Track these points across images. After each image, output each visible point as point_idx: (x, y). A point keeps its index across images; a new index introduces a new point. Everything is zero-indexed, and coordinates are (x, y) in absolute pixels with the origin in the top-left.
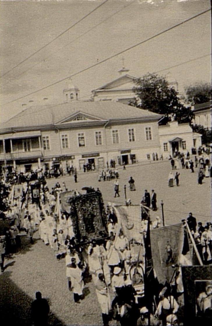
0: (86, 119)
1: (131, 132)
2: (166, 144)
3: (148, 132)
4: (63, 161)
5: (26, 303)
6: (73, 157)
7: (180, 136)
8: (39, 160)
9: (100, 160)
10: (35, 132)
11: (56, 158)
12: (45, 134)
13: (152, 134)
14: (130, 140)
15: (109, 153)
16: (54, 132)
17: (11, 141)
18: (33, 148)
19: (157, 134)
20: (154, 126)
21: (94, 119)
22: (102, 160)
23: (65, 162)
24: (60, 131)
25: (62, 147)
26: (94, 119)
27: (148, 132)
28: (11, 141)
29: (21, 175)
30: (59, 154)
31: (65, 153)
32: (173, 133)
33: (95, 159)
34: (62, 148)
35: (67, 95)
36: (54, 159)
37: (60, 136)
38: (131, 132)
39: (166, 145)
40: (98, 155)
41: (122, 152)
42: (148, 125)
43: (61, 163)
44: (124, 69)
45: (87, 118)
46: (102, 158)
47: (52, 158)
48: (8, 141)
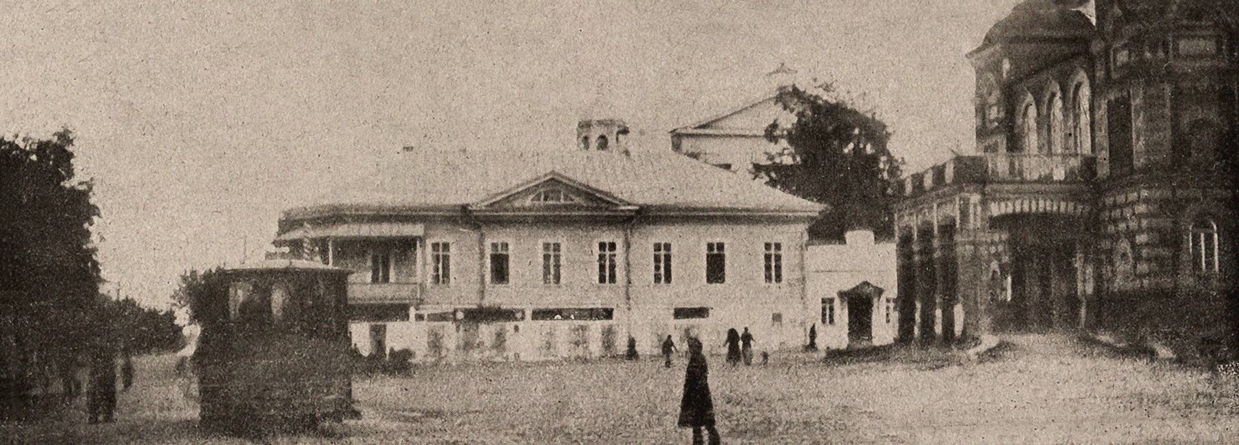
2: (831, 300)
6: (519, 315)
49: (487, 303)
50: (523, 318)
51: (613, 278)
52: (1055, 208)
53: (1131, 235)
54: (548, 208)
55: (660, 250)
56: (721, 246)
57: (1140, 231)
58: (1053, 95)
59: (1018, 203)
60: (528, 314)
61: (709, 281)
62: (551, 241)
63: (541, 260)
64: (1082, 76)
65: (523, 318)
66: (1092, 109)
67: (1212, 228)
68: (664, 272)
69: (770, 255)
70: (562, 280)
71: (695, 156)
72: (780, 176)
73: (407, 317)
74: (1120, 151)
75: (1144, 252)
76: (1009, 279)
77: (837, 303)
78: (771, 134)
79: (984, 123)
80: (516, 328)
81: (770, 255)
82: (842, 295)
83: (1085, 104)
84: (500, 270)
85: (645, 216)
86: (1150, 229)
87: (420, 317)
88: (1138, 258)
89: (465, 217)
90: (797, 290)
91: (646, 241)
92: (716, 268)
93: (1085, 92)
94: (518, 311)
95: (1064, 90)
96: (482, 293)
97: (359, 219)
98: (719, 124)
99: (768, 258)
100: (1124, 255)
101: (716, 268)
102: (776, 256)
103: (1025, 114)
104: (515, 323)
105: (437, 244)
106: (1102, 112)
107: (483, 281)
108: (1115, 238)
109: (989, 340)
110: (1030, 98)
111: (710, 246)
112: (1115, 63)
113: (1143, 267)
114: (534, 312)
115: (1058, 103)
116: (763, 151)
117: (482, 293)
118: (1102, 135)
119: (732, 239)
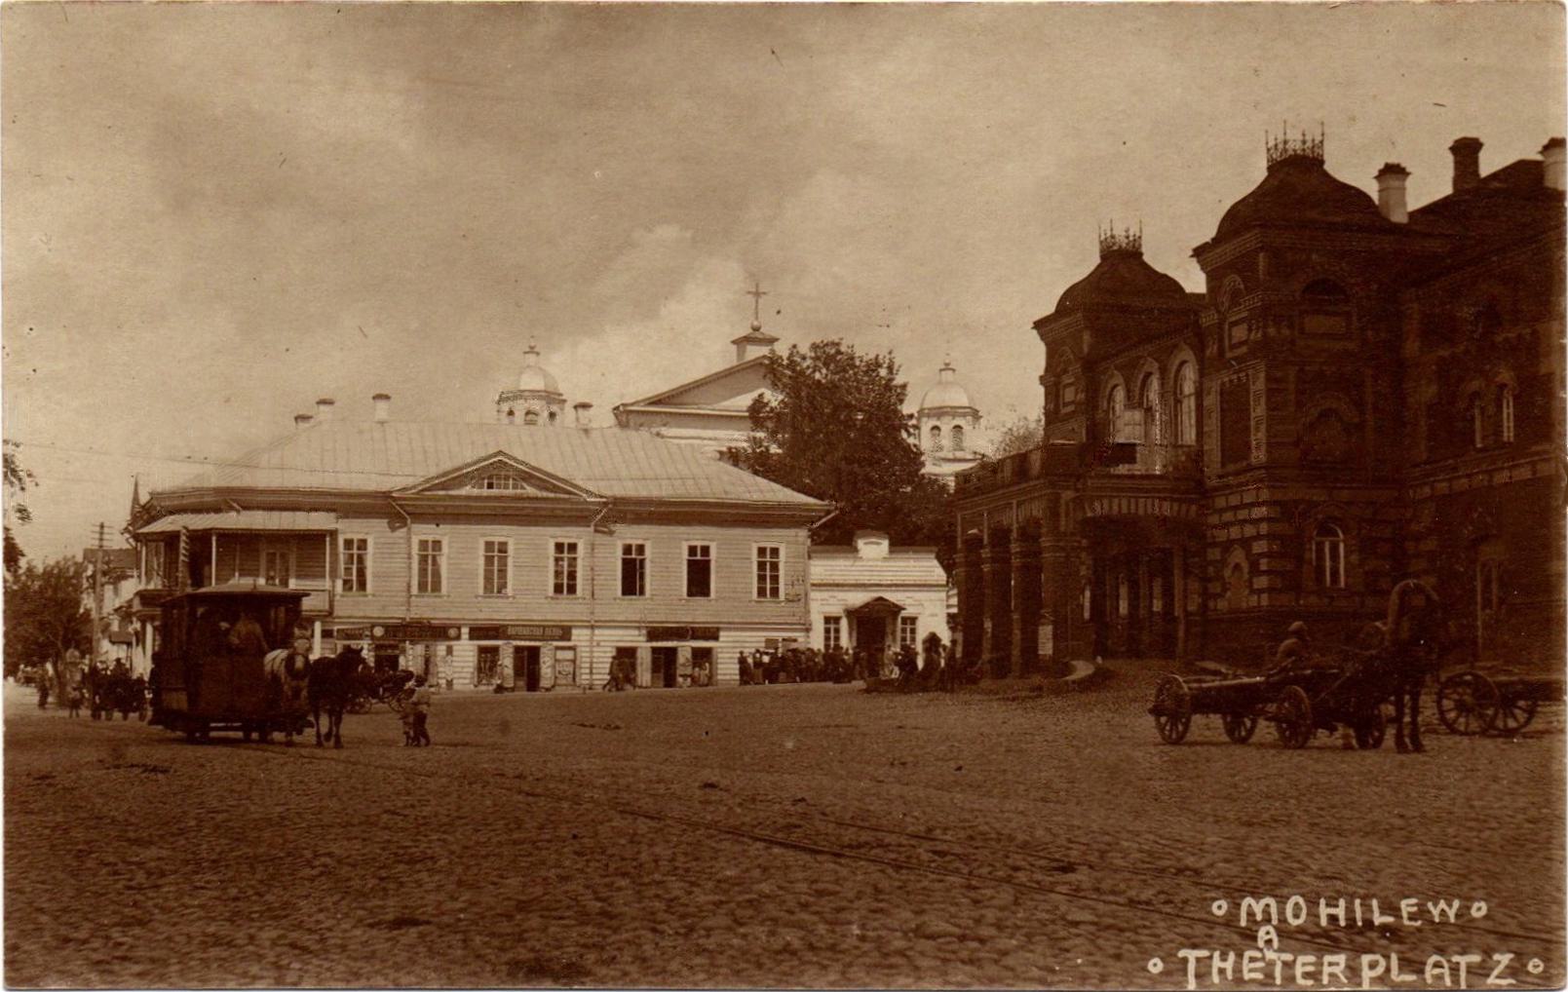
0: (523, 488)
1: (497, 555)
2: (837, 620)
3: (768, 566)
4: (412, 642)
5: (1271, 964)
6: (452, 632)
7: (892, 597)
8: (318, 627)
9: (560, 655)
10: (275, 514)
11: (387, 627)
12: (350, 529)
13: (781, 573)
14: (558, 589)
15: (597, 632)
16: (384, 522)
17: (214, 538)
18: (298, 577)
19: (801, 578)
20: (790, 543)
21: (601, 497)
22: (569, 655)
23: (420, 649)
24: (412, 522)
25: (415, 583)
26: (601, 497)
27: (768, 566)
28: (214, 538)
29: (758, 655)
30: (397, 613)
31: (426, 609)
32: (865, 579)
33: (542, 650)
34: (415, 590)
35: (936, 428)
36: (378, 632)
37: (409, 540)
38: (497, 555)
39: (832, 627)
40: (565, 633)
41: (654, 634)
42: (771, 537)
43: (404, 651)
44: (757, 335)
45: (525, 485)
46: (573, 648)
47: (373, 626)
48: (200, 538)
50: (458, 637)
52: (1115, 508)
53: (1246, 543)
55: (562, 552)
56: (706, 550)
57: (1258, 537)
58: (1149, 375)
59: (1124, 503)
61: (690, 594)
63: (482, 561)
64: (1187, 354)
65: (458, 637)
66: (1199, 394)
67: (1338, 536)
68: (632, 578)
69: (764, 563)
70: (369, 586)
71: (975, 453)
72: (760, 464)
74: (1235, 448)
75: (1264, 565)
76: (1088, 594)
77: (844, 624)
78: (756, 414)
79: (1057, 405)
80: (450, 651)
83: (1189, 388)
86: (1271, 537)
88: (1255, 570)
89: (393, 509)
92: (699, 578)
93: (1190, 374)
94: (451, 626)
95: (1163, 371)
98: (686, 398)
100: (1237, 567)
101: (699, 578)
102: (772, 564)
103: (1111, 398)
104: (447, 643)
106: (1212, 400)
108: (1227, 546)
109: (1082, 669)
110: (1118, 379)
111: (692, 550)
112: (1230, 340)
113: (1262, 582)
115: (1155, 384)
116: (739, 438)
118: (1213, 424)
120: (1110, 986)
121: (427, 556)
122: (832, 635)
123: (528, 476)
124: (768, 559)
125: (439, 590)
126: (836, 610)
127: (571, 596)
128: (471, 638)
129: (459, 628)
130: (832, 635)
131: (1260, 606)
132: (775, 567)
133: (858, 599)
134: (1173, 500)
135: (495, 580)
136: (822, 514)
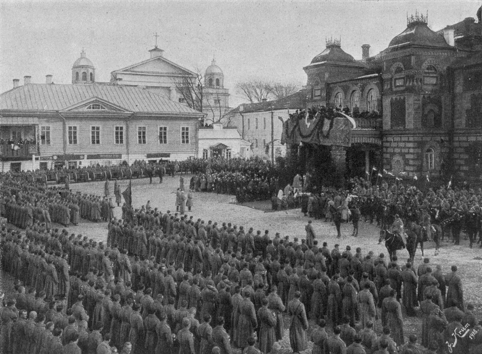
6: (81, 157)
36: (55, 158)
49: (67, 152)
50: (84, 159)
51: (122, 142)
54: (94, 112)
60: (86, 156)
62: (163, 126)
65: (84, 159)
69: (141, 132)
70: (78, 142)
73: (31, 159)
81: (141, 132)
82: (211, 148)
84: (73, 140)
85: (134, 117)
87: (37, 159)
89: (56, 116)
90: (194, 146)
91: (135, 127)
92: (163, 138)
96: (64, 148)
97: (128, 74)
99: (117, 133)
101: (163, 138)
102: (143, 132)
105: (141, 127)
107: (65, 143)
114: (88, 156)
117: (64, 148)
119: (168, 125)
120: (477, 1)
121: (94, 132)
122: (205, 155)
123: (111, 107)
124: (163, 131)
125: (122, 143)
126: (207, 147)
127: (121, 144)
128: (88, 159)
129: (84, 156)
130: (205, 155)
131: (453, 141)
132: (187, 133)
133: (214, 143)
134: (374, 137)
135: (96, 140)
136: (108, 106)
